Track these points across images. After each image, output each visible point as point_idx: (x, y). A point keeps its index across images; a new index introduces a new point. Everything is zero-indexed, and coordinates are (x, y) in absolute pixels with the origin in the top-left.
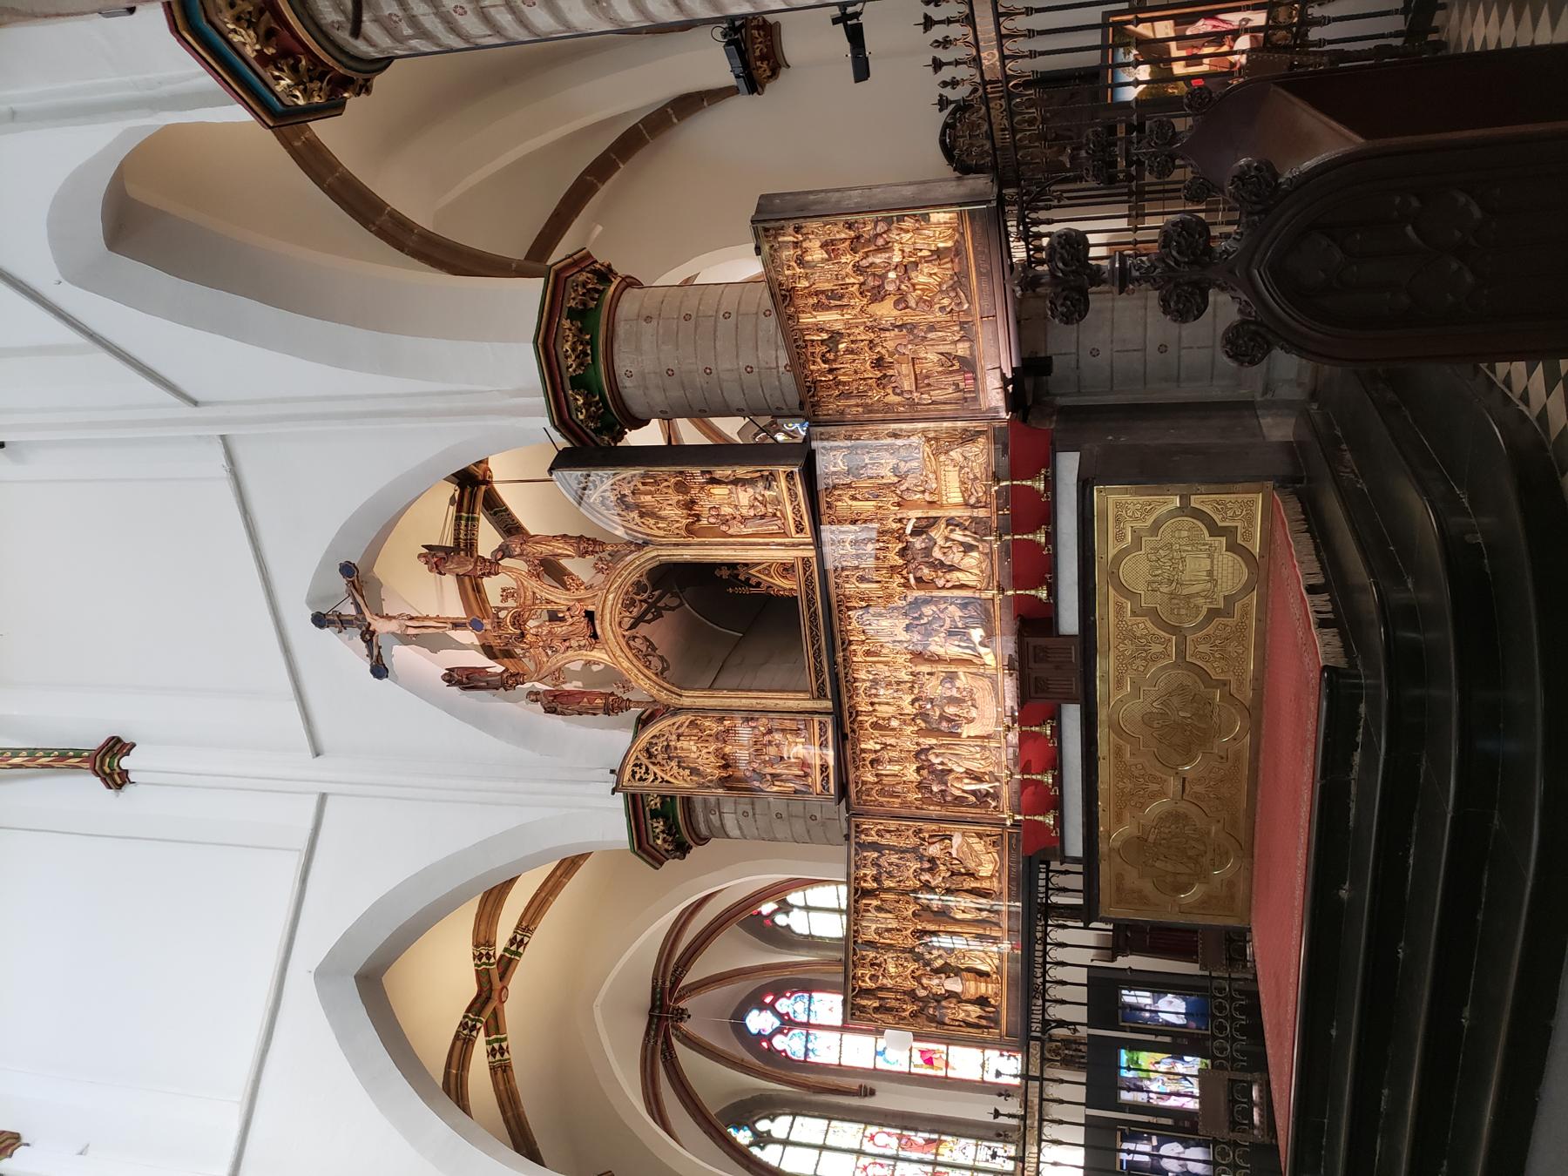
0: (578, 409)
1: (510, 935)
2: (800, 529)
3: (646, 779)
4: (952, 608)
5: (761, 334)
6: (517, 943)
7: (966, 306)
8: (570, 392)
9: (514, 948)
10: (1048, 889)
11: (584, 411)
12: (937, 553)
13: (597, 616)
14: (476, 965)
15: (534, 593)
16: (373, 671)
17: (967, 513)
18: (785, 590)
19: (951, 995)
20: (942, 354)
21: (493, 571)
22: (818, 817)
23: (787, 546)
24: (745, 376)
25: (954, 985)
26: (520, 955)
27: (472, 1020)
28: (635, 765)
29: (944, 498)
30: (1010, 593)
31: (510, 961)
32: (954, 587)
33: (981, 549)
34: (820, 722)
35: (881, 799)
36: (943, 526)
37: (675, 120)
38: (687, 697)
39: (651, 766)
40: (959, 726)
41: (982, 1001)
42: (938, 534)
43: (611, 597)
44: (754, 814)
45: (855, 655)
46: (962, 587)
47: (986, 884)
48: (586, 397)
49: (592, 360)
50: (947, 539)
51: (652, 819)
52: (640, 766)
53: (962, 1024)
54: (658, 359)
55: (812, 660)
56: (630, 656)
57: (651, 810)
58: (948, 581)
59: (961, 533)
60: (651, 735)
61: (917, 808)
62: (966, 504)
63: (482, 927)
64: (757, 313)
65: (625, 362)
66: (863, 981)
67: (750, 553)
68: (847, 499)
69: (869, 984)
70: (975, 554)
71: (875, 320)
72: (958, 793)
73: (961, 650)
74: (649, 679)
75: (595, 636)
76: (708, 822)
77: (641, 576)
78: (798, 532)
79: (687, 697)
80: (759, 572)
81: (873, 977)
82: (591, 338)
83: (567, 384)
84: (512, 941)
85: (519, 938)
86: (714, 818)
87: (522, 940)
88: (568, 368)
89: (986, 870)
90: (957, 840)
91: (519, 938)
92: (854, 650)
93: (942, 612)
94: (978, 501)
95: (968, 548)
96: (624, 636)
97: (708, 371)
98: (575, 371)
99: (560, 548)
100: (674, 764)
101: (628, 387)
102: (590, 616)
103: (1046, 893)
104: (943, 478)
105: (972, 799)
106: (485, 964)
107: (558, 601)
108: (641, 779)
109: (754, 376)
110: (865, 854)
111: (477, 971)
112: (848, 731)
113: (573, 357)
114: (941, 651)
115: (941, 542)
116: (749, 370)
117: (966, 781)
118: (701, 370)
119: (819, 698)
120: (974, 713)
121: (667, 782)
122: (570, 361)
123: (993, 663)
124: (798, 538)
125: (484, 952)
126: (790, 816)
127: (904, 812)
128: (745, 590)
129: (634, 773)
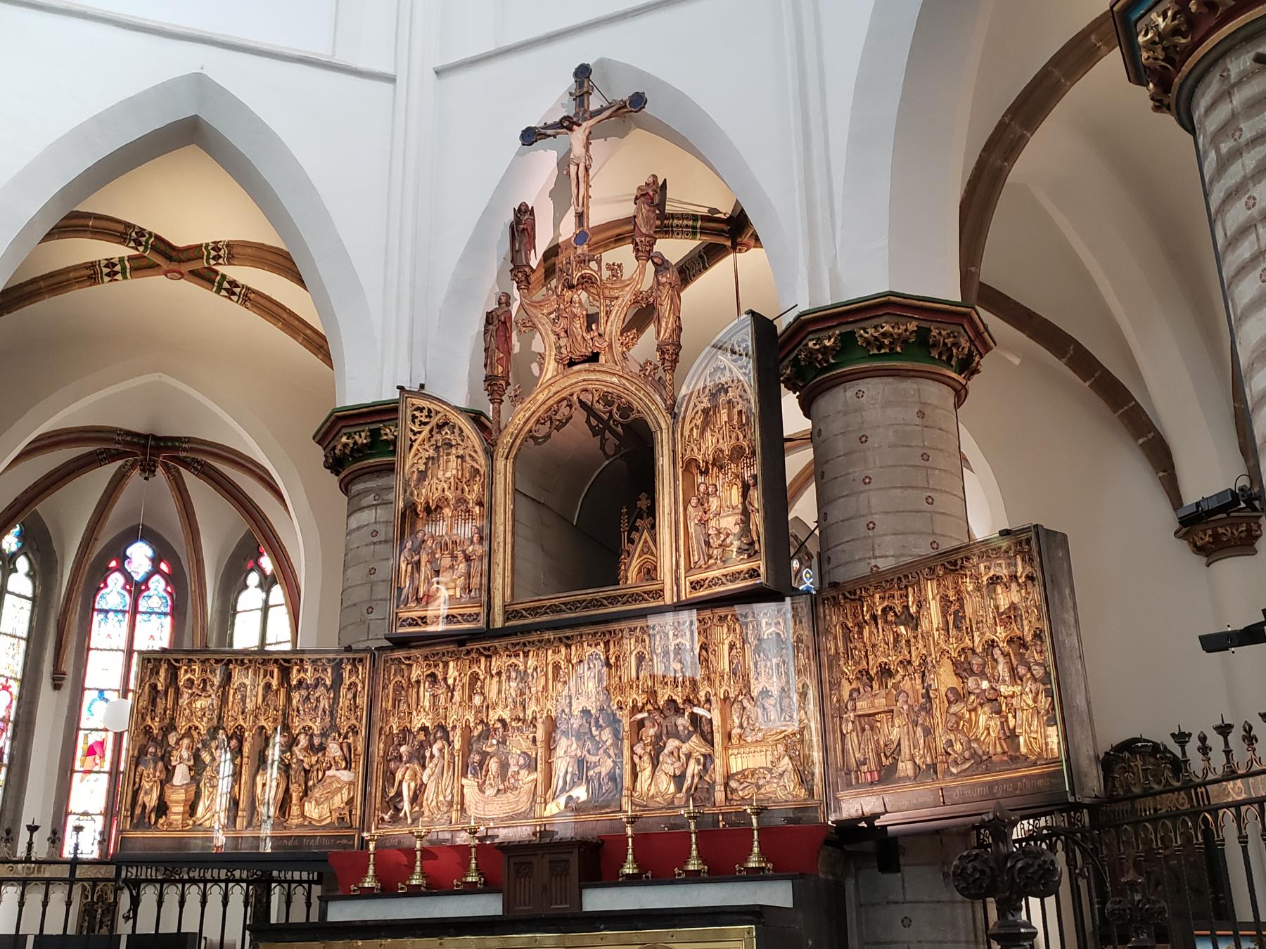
0: (819, 341)
1: (240, 281)
2: (695, 585)
3: (414, 423)
4: (609, 763)
5: (911, 538)
6: (232, 289)
7: (954, 770)
8: (837, 332)
9: (226, 285)
10: (290, 882)
11: (818, 347)
12: (672, 744)
13: (594, 366)
14: (207, 245)
15: (617, 298)
16: (529, 129)
17: (719, 778)
18: (626, 571)
19: (170, 772)
20: (899, 744)
21: (640, 254)
22: (372, 616)
23: (676, 571)
24: (863, 522)
25: (181, 775)
26: (218, 292)
27: (147, 242)
28: (430, 411)
29: (735, 751)
30: (629, 831)
31: (213, 282)
32: (634, 765)
33: (678, 795)
34: (478, 615)
35: (391, 687)
36: (703, 750)
37: (1141, 441)
38: (506, 465)
39: (428, 428)
40: (475, 775)
41: (162, 808)
42: (695, 743)
43: (615, 380)
44: (374, 543)
45: (554, 652)
46: (635, 775)
47: (295, 810)
48: (832, 348)
49: (874, 355)
50: (689, 756)
51: (370, 430)
52: (429, 416)
53: (137, 785)
54: (878, 426)
55: (548, 603)
56: (551, 402)
57: (380, 429)
58: (640, 757)
59: (696, 772)
60: (462, 426)
61: (381, 728)
62: (729, 777)
63: (249, 251)
64: (934, 533)
65: (874, 389)
66: (186, 672)
67: (667, 530)
68: (730, 638)
69: (183, 677)
70: (672, 789)
71: (934, 666)
72: (398, 776)
73: (562, 775)
74: (525, 423)
75: (572, 363)
76: (366, 492)
77: (639, 412)
78: (691, 583)
79: (506, 465)
80: (646, 542)
81: (191, 681)
82: (897, 352)
83: (848, 328)
84: (234, 284)
85: (237, 290)
86: (370, 499)
87: (234, 294)
88: (864, 329)
89: (312, 810)
90: (345, 776)
91: (237, 290)
92: (559, 651)
93: (605, 751)
94: (734, 791)
95: (679, 779)
96: (572, 395)
97: (867, 480)
98: (861, 336)
99: (667, 323)
100: (431, 452)
101: (844, 395)
102: (594, 358)
103: (286, 881)
104: (759, 749)
105: (392, 793)
106: (209, 254)
107: (609, 324)
108: (414, 417)
109: (863, 531)
110: (329, 670)
111: (201, 245)
112: (469, 647)
113: (876, 334)
114: (560, 751)
115: (685, 748)
116: (871, 526)
117: (413, 785)
118: (867, 473)
119: (505, 612)
120: (490, 792)
121: (411, 446)
122: (871, 331)
123: (547, 813)
124: (685, 584)
125: (222, 253)
126: (373, 584)
127: (377, 714)
128: (625, 526)
129: (421, 409)
